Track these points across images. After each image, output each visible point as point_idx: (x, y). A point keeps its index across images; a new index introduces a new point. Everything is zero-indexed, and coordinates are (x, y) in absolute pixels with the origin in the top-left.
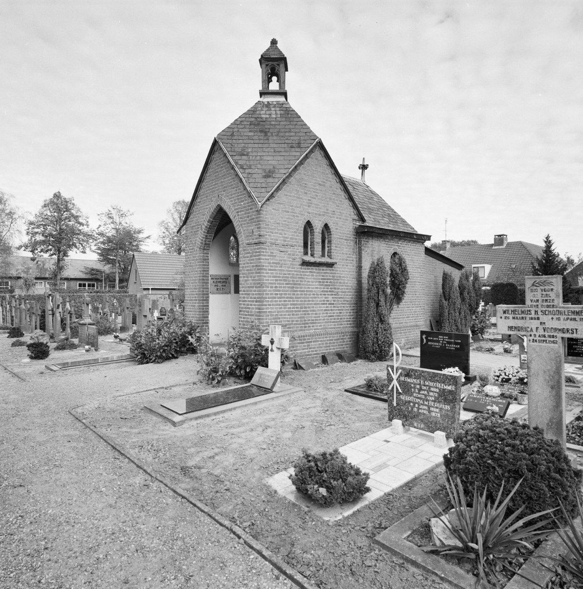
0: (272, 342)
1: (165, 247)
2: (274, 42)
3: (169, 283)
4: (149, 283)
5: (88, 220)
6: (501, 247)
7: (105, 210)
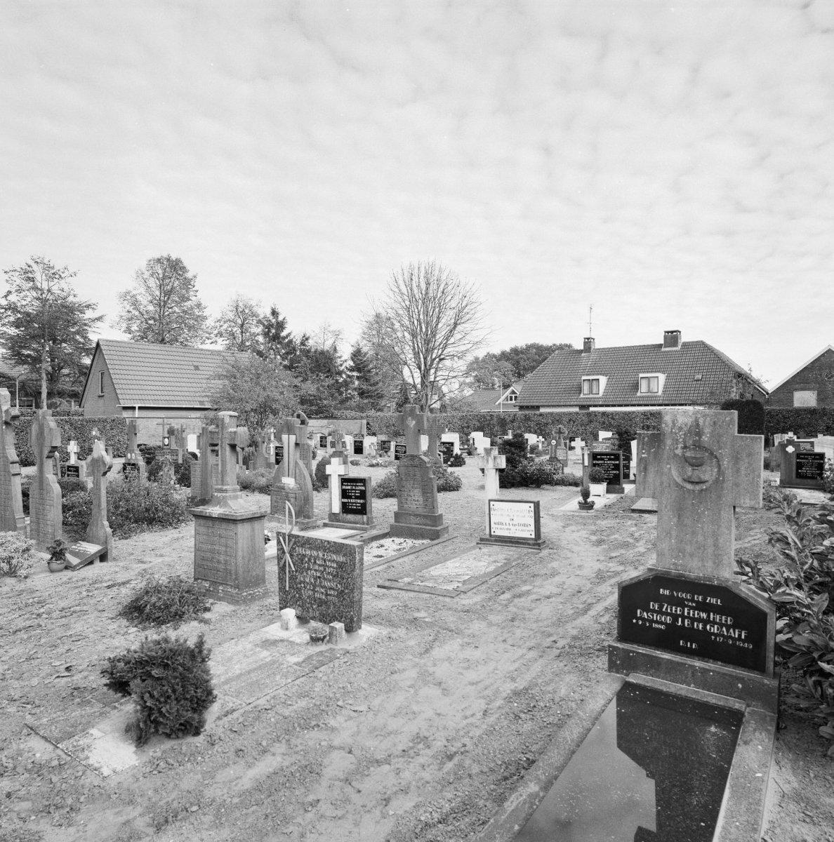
1: (130, 336)
4: (134, 397)
6: (674, 349)
7: (20, 262)
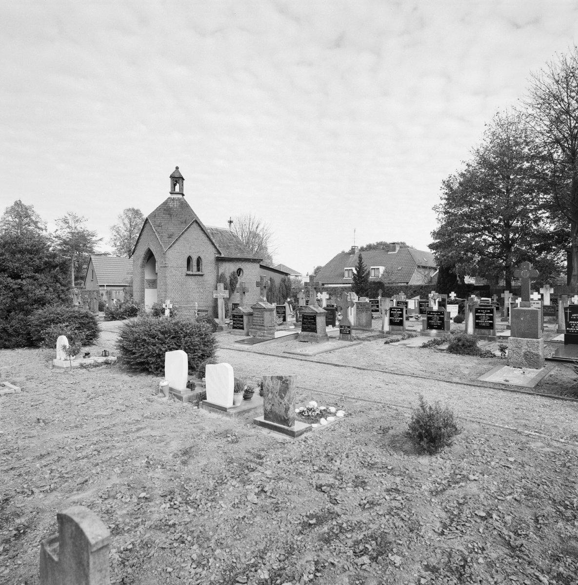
0: (166, 306)
1: (116, 248)
2: (177, 168)
3: (121, 281)
5: (46, 225)
6: (394, 253)
7: (62, 215)
